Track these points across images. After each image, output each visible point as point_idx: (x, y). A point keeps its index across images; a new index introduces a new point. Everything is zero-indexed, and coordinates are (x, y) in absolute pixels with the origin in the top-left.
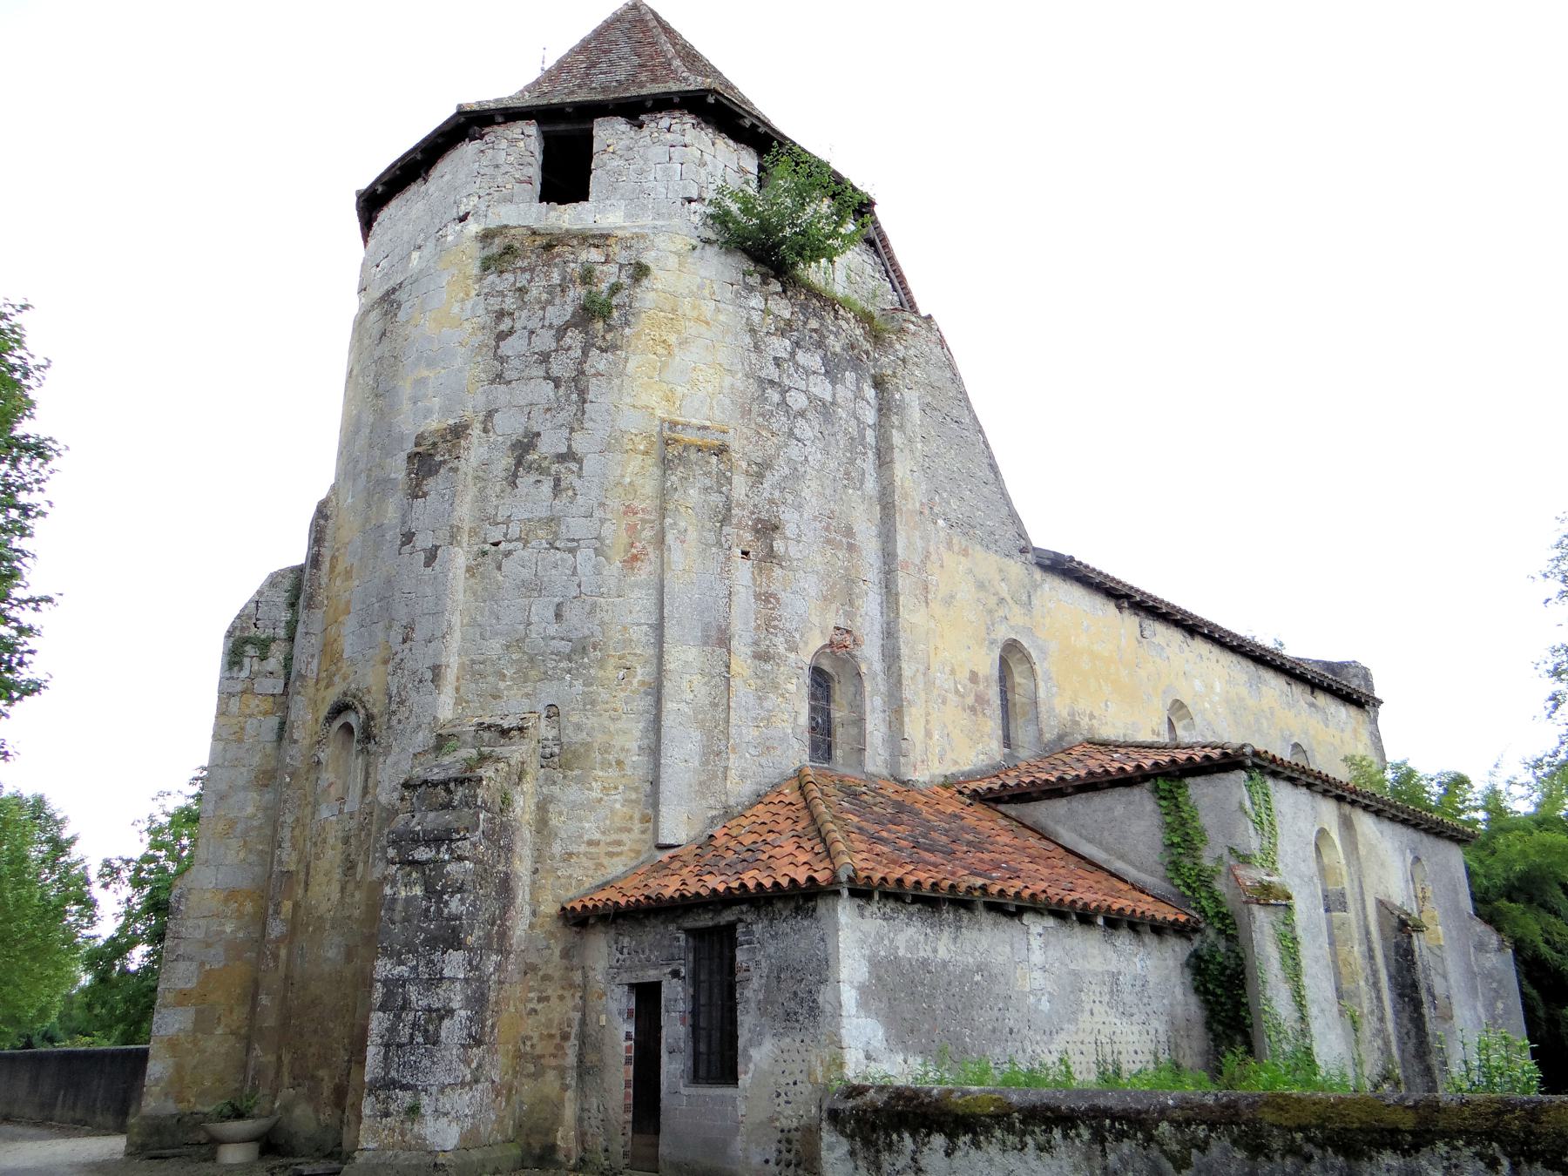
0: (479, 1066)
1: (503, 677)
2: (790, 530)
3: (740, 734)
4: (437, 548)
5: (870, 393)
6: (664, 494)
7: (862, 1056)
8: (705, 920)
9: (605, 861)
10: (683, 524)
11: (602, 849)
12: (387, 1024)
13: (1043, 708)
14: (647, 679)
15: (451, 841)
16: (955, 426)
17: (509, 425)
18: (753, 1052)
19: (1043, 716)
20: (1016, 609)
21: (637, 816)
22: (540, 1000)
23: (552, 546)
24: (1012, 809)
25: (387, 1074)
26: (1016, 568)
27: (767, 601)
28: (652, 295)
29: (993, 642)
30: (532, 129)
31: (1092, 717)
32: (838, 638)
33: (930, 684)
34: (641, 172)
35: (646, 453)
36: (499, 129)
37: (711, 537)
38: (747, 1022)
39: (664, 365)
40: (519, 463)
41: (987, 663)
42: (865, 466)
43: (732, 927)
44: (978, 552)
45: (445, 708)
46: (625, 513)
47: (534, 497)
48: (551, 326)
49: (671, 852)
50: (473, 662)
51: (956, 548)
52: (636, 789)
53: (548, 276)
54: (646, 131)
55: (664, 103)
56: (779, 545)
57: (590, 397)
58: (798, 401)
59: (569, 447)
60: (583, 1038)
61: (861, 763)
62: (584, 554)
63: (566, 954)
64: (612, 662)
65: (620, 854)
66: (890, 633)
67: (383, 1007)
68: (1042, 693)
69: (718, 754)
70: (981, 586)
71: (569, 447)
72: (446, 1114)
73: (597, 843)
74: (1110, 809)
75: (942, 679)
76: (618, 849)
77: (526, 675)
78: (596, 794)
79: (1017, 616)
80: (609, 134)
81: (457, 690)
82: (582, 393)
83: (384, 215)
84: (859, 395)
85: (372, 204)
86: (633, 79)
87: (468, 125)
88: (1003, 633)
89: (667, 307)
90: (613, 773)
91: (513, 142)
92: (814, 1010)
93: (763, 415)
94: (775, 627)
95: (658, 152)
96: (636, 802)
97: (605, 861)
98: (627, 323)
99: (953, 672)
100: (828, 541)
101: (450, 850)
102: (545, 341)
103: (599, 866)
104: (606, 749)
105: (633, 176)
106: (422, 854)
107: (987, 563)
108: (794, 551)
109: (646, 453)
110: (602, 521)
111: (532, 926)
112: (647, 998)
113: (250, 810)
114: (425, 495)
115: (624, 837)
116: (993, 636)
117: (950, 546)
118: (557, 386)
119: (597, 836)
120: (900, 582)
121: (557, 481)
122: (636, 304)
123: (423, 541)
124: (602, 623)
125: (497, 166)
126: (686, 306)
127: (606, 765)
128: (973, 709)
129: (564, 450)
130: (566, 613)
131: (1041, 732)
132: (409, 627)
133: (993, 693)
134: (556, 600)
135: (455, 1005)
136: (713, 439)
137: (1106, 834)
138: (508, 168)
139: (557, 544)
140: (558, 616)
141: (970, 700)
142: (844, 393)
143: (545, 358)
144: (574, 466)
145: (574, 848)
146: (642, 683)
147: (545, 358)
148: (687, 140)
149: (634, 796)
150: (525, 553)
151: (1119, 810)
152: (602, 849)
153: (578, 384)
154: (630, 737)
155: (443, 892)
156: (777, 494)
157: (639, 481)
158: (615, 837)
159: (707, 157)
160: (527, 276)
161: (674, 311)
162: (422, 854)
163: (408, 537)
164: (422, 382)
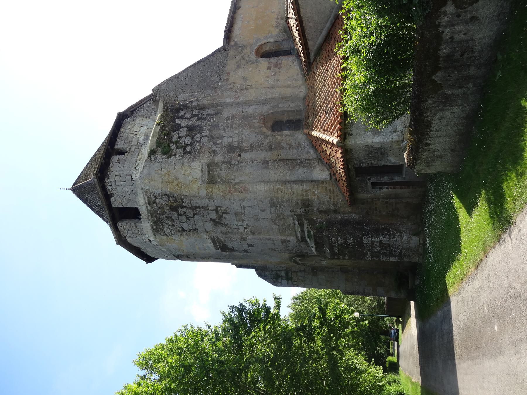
0: (396, 230)
1: (283, 225)
2: (230, 140)
3: (295, 154)
4: (247, 244)
5: (182, 113)
6: (223, 182)
7: (395, 134)
8: (353, 173)
9: (335, 194)
10: (233, 177)
11: (332, 195)
12: (384, 257)
13: (277, 39)
14: (281, 184)
15: (332, 243)
16: (187, 79)
17: (209, 226)
18: (393, 162)
19: (279, 39)
20: (245, 52)
21: (322, 185)
22: (376, 210)
23: (244, 213)
24: (312, 58)
25: (397, 256)
26: (231, 53)
27: (253, 147)
28: (163, 189)
29: (256, 60)
30: (119, 224)
31: (277, 18)
32: (262, 121)
33: (273, 87)
34: (126, 193)
35: (212, 188)
36: (122, 233)
37: (236, 168)
38: (383, 163)
39: (184, 184)
40: (221, 224)
41: (264, 63)
42: (206, 114)
43: (355, 168)
44: (228, 68)
45: (292, 239)
46: (231, 193)
47: (229, 219)
48: (178, 217)
49: (332, 175)
50: (280, 232)
51: (228, 77)
52: (314, 186)
53: (163, 219)
54: (113, 192)
55: (103, 188)
56: (235, 144)
57: (198, 205)
58: (188, 140)
59: (214, 210)
60: (387, 198)
61: (301, 111)
62: (245, 204)
63: (363, 204)
64: (276, 195)
65: (333, 190)
66: (259, 103)
67: (379, 257)
68: (272, 40)
69: (302, 162)
70: (238, 67)
71: (214, 210)
72: (409, 241)
73: (330, 196)
74: (310, 27)
75: (271, 81)
76: (332, 190)
77: (283, 218)
78: (316, 197)
79: (248, 51)
80: (116, 203)
81: (288, 236)
82: (196, 207)
83: (152, 256)
84: (182, 117)
85: (149, 259)
86: (97, 194)
87: (121, 240)
88: (253, 57)
89: (167, 184)
90: (309, 193)
91: (124, 229)
92: (381, 148)
93: (195, 152)
94: (261, 144)
95: (119, 189)
96: (318, 186)
97: (335, 194)
98: (174, 196)
99: (268, 77)
100: (232, 127)
101: (335, 243)
102: (183, 218)
103: (337, 195)
104: (302, 195)
105: (128, 195)
106: (336, 249)
107: (231, 65)
108: (236, 139)
109: (212, 188)
110: (235, 200)
111: (355, 213)
112: (374, 185)
113: (324, 277)
114: (233, 247)
115: (328, 189)
116: (255, 61)
117: (227, 80)
118: (196, 214)
119: (328, 196)
120: (241, 100)
121: (224, 213)
122: (167, 193)
123: (246, 247)
124: (265, 198)
125: (133, 233)
126: (165, 178)
127: (307, 195)
128: (280, 68)
129: (214, 212)
130: (263, 208)
131: (285, 40)
132: (271, 249)
133: (274, 60)
134: (259, 211)
135: (378, 240)
136: (205, 168)
137: (319, 28)
138: (133, 230)
139: (243, 212)
140: (264, 211)
141: (277, 69)
142: (183, 123)
143: (188, 218)
144: (219, 209)
145: (332, 203)
146: (282, 186)
147: (188, 218)
148: (113, 180)
149: (316, 187)
150: (247, 220)
151: (311, 24)
152: (332, 195)
153: (194, 208)
154: (298, 188)
155: (347, 245)
156: (219, 146)
157: (221, 190)
158: (328, 192)
159: (117, 174)
160: (164, 224)
161: (167, 182)
162: (336, 249)
163: (245, 251)
164: (200, 248)
